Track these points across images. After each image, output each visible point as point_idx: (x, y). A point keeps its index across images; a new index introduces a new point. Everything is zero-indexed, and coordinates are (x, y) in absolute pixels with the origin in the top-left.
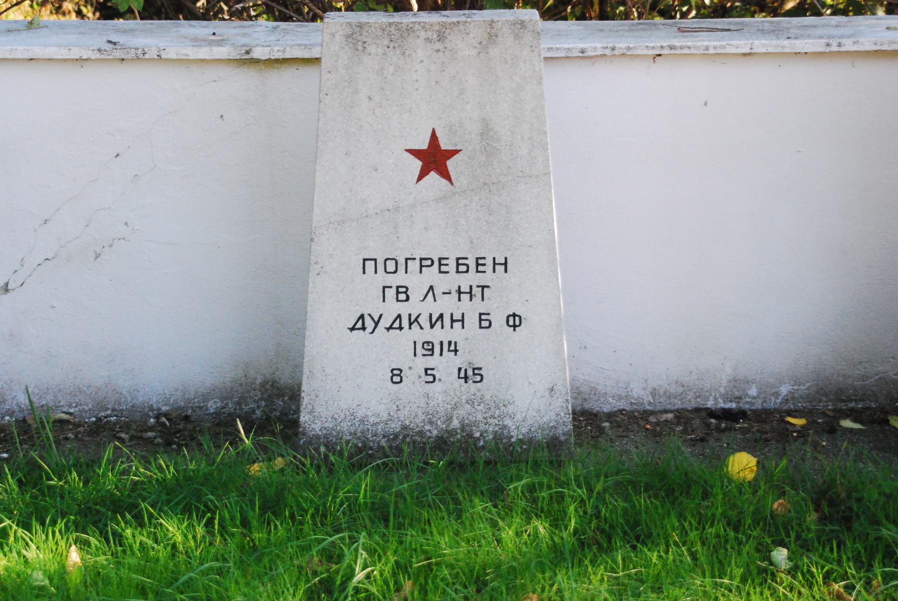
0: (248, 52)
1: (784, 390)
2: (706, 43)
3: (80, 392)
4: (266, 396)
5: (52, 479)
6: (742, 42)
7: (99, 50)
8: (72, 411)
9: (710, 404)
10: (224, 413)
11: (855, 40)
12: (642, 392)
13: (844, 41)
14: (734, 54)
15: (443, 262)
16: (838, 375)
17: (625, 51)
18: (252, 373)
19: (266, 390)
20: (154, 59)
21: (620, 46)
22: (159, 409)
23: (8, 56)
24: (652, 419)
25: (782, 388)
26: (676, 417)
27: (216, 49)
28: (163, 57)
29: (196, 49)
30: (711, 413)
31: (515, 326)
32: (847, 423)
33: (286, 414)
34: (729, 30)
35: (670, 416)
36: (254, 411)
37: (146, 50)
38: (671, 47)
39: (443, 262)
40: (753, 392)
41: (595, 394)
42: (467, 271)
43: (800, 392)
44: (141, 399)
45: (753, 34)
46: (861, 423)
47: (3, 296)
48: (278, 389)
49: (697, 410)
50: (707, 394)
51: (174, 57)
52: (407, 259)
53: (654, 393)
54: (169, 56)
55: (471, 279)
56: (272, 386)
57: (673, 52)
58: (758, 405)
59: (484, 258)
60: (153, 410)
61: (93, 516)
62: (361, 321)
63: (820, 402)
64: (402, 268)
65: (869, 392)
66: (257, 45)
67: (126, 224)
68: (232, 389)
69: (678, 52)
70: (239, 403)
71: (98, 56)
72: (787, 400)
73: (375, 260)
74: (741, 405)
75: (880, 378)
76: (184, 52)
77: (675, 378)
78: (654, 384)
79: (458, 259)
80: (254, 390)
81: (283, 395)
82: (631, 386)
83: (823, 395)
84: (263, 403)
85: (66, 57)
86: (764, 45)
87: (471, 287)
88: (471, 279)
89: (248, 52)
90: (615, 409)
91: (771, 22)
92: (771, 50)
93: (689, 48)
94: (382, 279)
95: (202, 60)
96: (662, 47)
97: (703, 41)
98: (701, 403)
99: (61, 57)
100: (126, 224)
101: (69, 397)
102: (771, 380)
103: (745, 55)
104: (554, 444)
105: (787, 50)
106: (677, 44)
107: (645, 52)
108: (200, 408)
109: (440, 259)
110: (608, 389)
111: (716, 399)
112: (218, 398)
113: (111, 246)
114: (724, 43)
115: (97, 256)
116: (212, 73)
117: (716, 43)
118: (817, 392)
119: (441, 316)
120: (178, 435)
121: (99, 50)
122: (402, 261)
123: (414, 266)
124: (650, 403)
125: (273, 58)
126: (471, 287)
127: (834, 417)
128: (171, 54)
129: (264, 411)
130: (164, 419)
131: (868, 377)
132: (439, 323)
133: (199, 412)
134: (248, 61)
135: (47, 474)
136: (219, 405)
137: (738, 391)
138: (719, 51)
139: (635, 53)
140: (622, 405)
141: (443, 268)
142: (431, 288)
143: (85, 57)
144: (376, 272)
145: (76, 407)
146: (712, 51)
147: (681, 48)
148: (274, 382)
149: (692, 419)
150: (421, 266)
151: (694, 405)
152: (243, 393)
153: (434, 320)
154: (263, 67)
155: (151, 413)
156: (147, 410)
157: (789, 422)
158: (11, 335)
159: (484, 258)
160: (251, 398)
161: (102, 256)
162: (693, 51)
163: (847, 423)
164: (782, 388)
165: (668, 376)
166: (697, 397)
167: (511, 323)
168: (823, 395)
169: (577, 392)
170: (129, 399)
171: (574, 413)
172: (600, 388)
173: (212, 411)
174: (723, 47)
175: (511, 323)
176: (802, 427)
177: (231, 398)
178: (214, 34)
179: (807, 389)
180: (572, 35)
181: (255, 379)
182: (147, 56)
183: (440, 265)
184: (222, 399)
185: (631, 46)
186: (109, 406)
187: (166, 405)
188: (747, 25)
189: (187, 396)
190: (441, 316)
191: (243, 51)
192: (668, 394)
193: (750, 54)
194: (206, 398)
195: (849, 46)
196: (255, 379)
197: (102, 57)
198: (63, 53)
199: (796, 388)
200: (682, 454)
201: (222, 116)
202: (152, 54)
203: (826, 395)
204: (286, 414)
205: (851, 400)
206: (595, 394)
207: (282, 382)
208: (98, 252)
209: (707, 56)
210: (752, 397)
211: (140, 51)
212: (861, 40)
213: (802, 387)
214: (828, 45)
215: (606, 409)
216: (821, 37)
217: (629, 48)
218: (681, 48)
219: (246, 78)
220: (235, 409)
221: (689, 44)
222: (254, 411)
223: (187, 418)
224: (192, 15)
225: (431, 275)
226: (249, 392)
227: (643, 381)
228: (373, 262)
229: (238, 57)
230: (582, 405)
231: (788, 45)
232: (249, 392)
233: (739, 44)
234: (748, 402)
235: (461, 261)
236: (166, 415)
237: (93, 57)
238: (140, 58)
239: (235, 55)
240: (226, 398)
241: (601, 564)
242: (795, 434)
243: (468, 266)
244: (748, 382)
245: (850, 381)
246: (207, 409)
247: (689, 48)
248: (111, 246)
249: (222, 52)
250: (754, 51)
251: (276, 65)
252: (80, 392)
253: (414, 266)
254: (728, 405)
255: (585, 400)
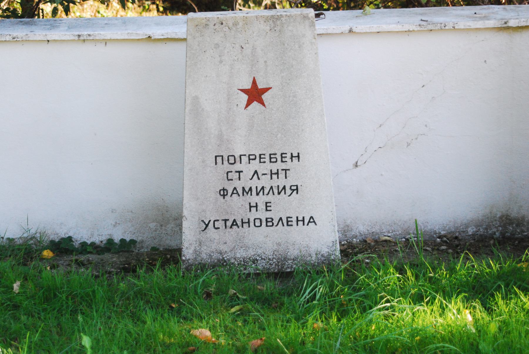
0: (506, 23)
3: (395, 224)
4: (502, 224)
5: (431, 273)
7: (419, 25)
8: (389, 235)
10: (477, 235)
18: (495, 210)
19: (503, 221)
20: (451, 29)
22: (440, 233)
23: (368, 31)
27: (487, 22)
28: (456, 27)
29: (476, 22)
33: (514, 235)
36: (495, 233)
37: (446, 24)
39: (262, 156)
42: (276, 162)
44: (429, 227)
47: (355, 169)
48: (510, 220)
51: (462, 27)
52: (241, 156)
54: (459, 27)
55: (279, 165)
56: (506, 218)
59: (286, 154)
60: (436, 234)
61: (479, 291)
62: (271, 191)
66: (511, 19)
67: (426, 126)
68: (482, 220)
70: (486, 229)
71: (419, 29)
73: (222, 156)
76: (468, 24)
79: (270, 155)
80: (496, 221)
81: (512, 224)
84: (501, 228)
85: (401, 30)
87: (278, 170)
88: (279, 165)
89: (506, 23)
94: (227, 167)
95: (477, 29)
99: (398, 30)
100: (426, 126)
101: (388, 227)
108: (463, 232)
109: (260, 155)
112: (474, 226)
113: (416, 139)
115: (408, 145)
120: (459, 248)
121: (419, 25)
123: (245, 159)
125: (520, 25)
126: (278, 170)
128: (461, 25)
129: (501, 233)
130: (445, 239)
132: (283, 191)
133: (463, 234)
134: (506, 28)
135: (430, 271)
136: (474, 230)
142: (256, 172)
143: (411, 30)
145: (392, 232)
148: (507, 215)
150: (249, 159)
152: (489, 223)
153: (280, 190)
154: (511, 31)
155: (435, 236)
156: (432, 233)
158: (358, 192)
159: (286, 154)
160: (493, 225)
161: (411, 145)
169: (344, 230)
170: (423, 227)
173: (470, 233)
177: (481, 226)
178: (475, 13)
180: (336, 20)
181: (496, 214)
182: (447, 28)
183: (260, 158)
184: (477, 226)
186: (411, 232)
187: (444, 230)
188: (492, 8)
189: (456, 225)
191: (503, 22)
194: (467, 226)
196: (496, 214)
197: (421, 29)
198: (399, 28)
201: (485, 61)
202: (450, 26)
204: (514, 235)
207: (512, 216)
208: (409, 142)
211: (443, 25)
219: (503, 38)
220: (484, 232)
222: (495, 233)
223: (456, 238)
224: (421, 5)
225: (255, 165)
226: (492, 222)
229: (500, 26)
232: (492, 222)
236: (445, 236)
237: (416, 29)
238: (443, 29)
239: (498, 24)
240: (478, 226)
241: (191, 336)
246: (467, 233)
248: (416, 139)
249: (491, 23)
251: (519, 30)
252: (395, 224)
253: (245, 159)
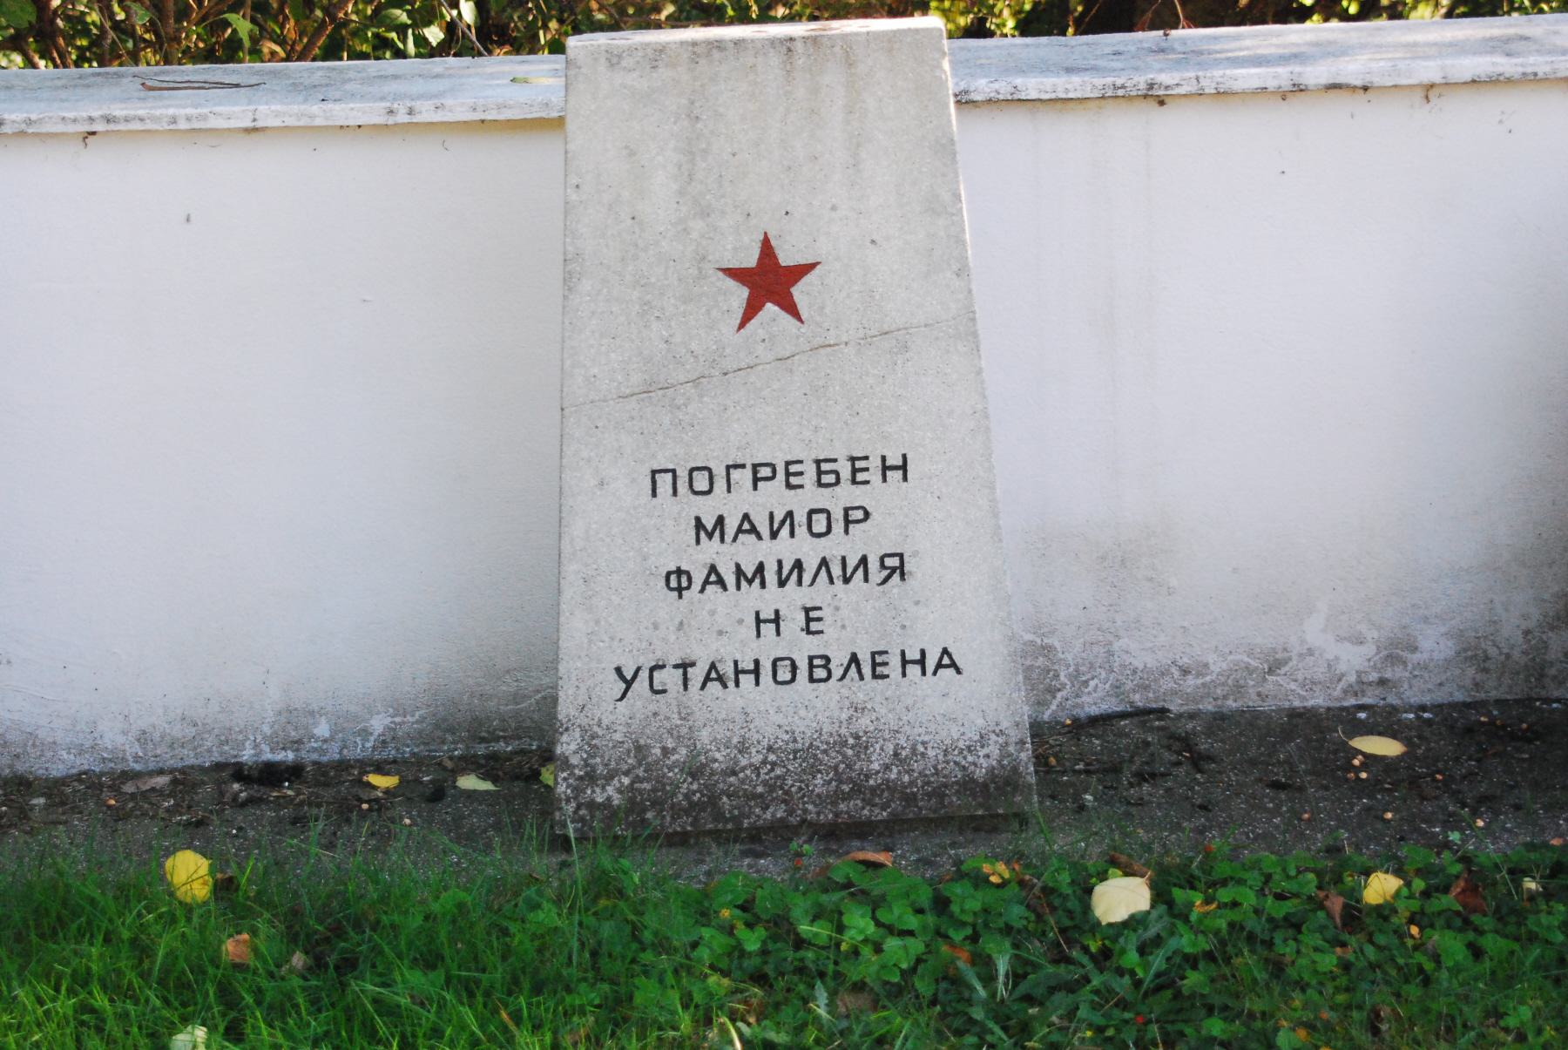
1: (378, 724)
2: (171, 111)
6: (236, 109)
9: (247, 755)
11: (438, 102)
12: (120, 739)
13: (417, 105)
14: (442, 123)
15: (793, 469)
16: (472, 695)
17: (23, 126)
21: (13, 117)
24: (129, 788)
25: (373, 722)
26: (175, 782)
30: (239, 772)
31: (680, 590)
32: (469, 782)
34: (237, 86)
35: (161, 781)
38: (108, 120)
40: (322, 730)
41: (34, 745)
42: (838, 482)
43: (406, 728)
45: (275, 95)
46: (495, 781)
49: (219, 767)
50: (240, 737)
53: (143, 738)
57: (112, 127)
58: (333, 754)
63: (443, 742)
64: (720, 484)
65: (528, 723)
69: (122, 127)
72: (384, 742)
73: (674, 471)
74: (303, 754)
75: (544, 698)
77: (179, 711)
78: (143, 724)
82: (100, 728)
83: (447, 730)
86: (277, 114)
90: (74, 771)
91: (322, 68)
92: (290, 122)
93: (142, 120)
96: (91, 119)
97: (168, 107)
98: (228, 753)
102: (352, 708)
103: (247, 130)
104: (1004, 782)
105: (319, 122)
106: (117, 113)
107: (60, 128)
110: (59, 736)
111: (256, 746)
114: (205, 111)
116: (1070, 132)
117: (189, 111)
118: (437, 726)
119: (864, 561)
122: (719, 471)
124: (137, 758)
127: (452, 771)
131: (525, 697)
132: (860, 572)
137: (296, 729)
138: (197, 125)
139: (44, 130)
140: (84, 763)
141: (794, 480)
144: (654, 494)
146: (183, 125)
147: (127, 120)
149: (203, 783)
150: (756, 480)
151: (216, 757)
153: (785, 572)
157: (369, 784)
162: (149, 126)
163: (469, 782)
164: (373, 722)
165: (166, 708)
166: (222, 744)
167: (674, 584)
168: (447, 730)
171: (1032, 726)
172: (42, 734)
174: (204, 118)
175: (674, 584)
176: (387, 791)
179: (417, 722)
183: (788, 474)
185: (34, 117)
190: (864, 561)
192: (168, 738)
193: (255, 130)
195: (426, 114)
199: (397, 719)
200: (72, 853)
203: (452, 730)
205: (497, 739)
206: (34, 745)
209: (178, 134)
210: (323, 738)
212: (449, 102)
213: (409, 718)
214: (391, 112)
215: (57, 771)
216: (382, 99)
217: (29, 122)
218: (127, 120)
221: (141, 112)
227: (121, 718)
228: (706, 474)
230: (11, 766)
231: (318, 113)
233: (231, 111)
234: (315, 750)
235: (824, 467)
242: (365, 806)
243: (837, 473)
244: (312, 713)
245: (492, 704)
247: (142, 120)
250: (259, 124)
253: (743, 477)
254: (279, 756)
255: (17, 756)
